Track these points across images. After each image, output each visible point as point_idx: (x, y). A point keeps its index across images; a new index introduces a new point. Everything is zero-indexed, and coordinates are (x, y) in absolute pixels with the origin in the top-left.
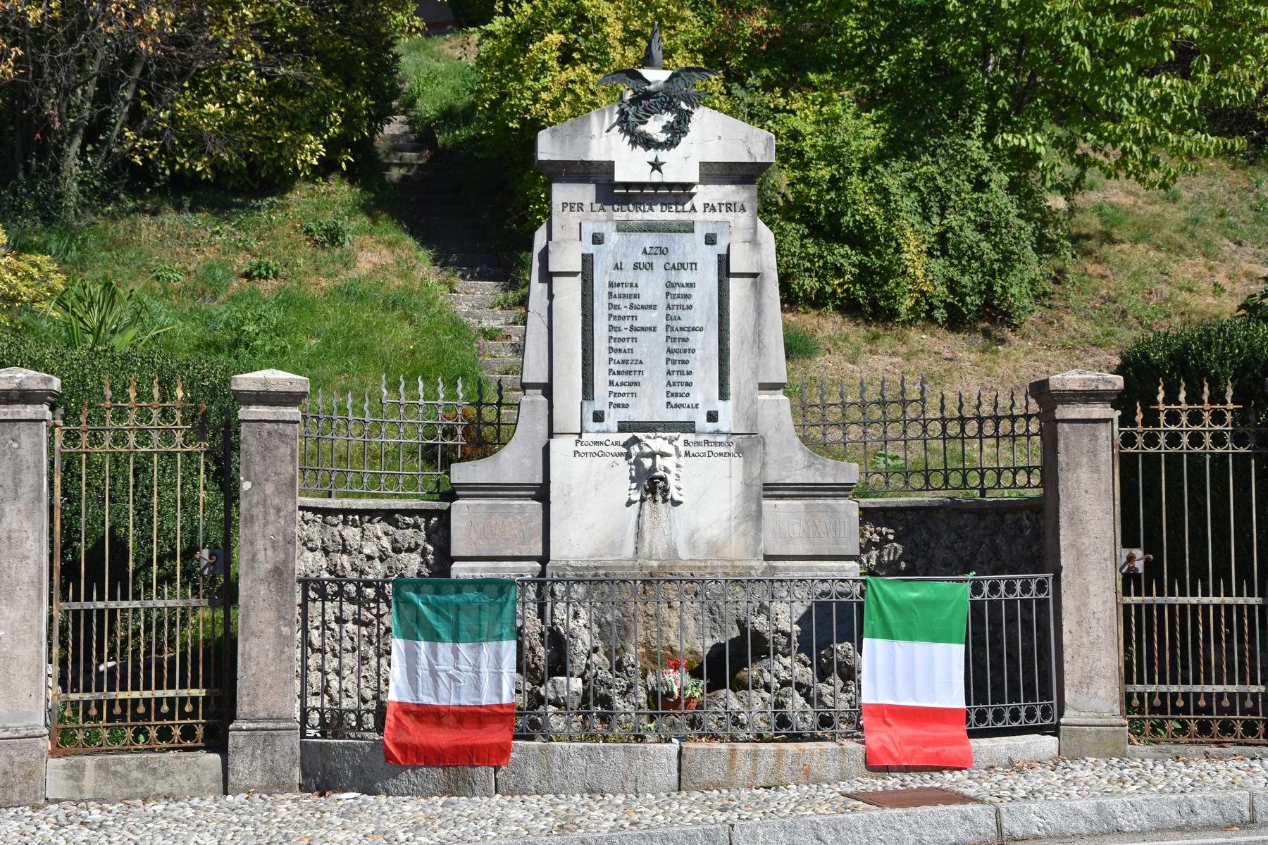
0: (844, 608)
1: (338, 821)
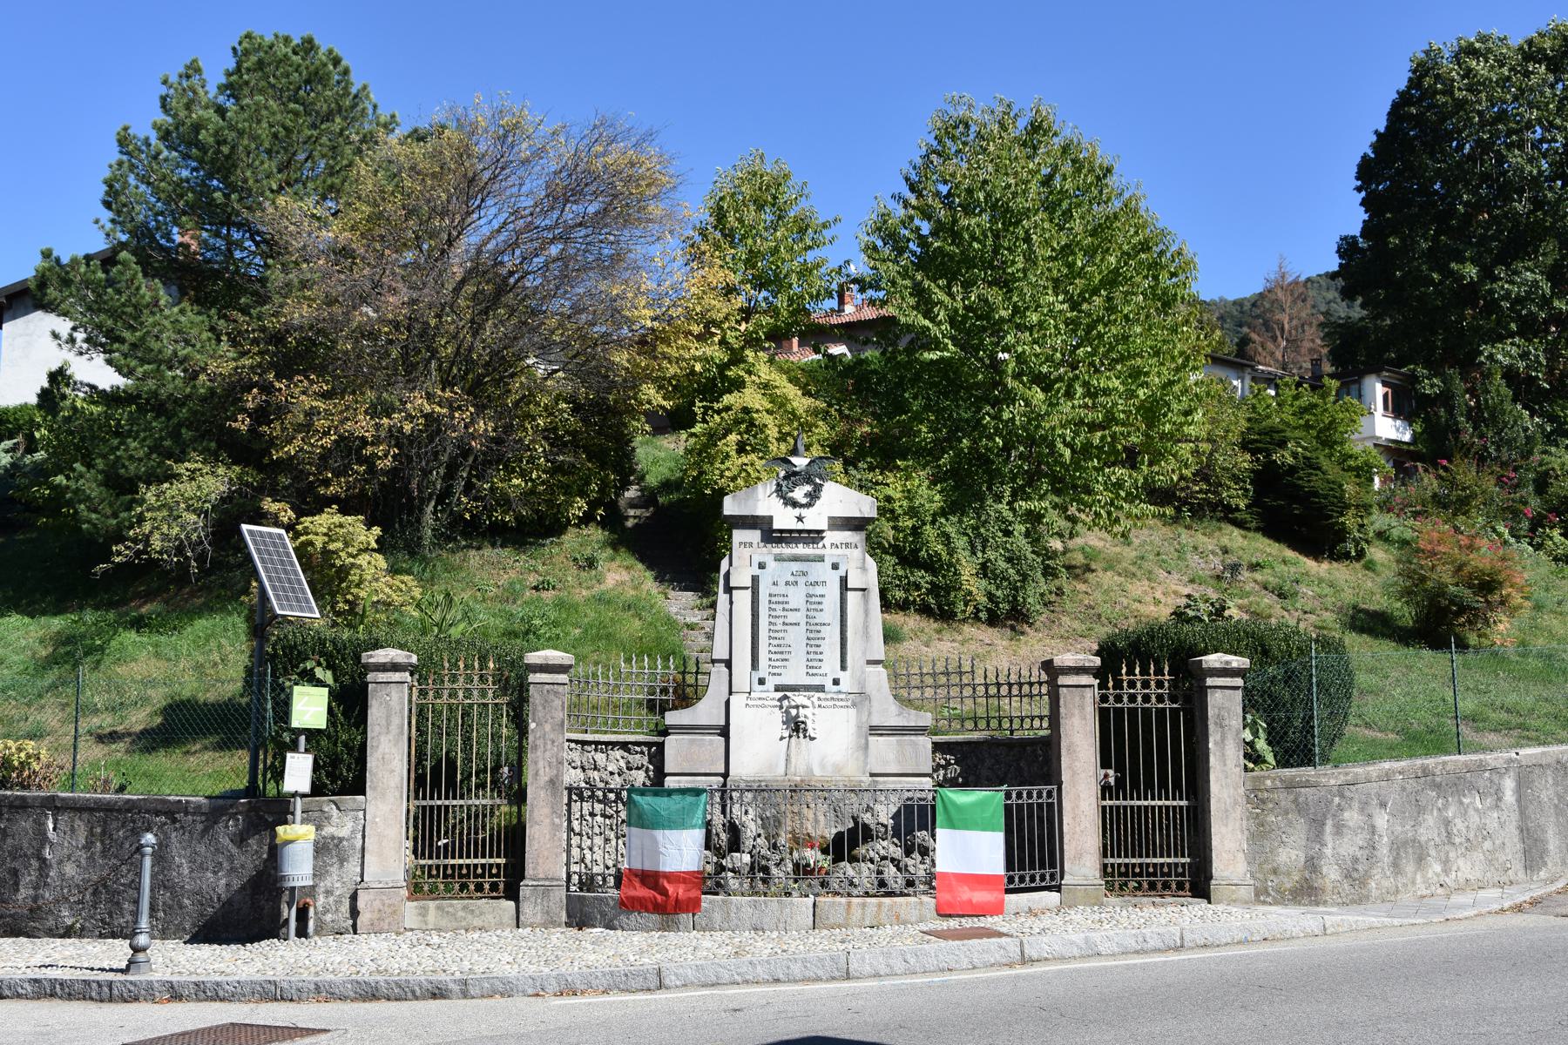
0: (922, 809)
1: (590, 947)
